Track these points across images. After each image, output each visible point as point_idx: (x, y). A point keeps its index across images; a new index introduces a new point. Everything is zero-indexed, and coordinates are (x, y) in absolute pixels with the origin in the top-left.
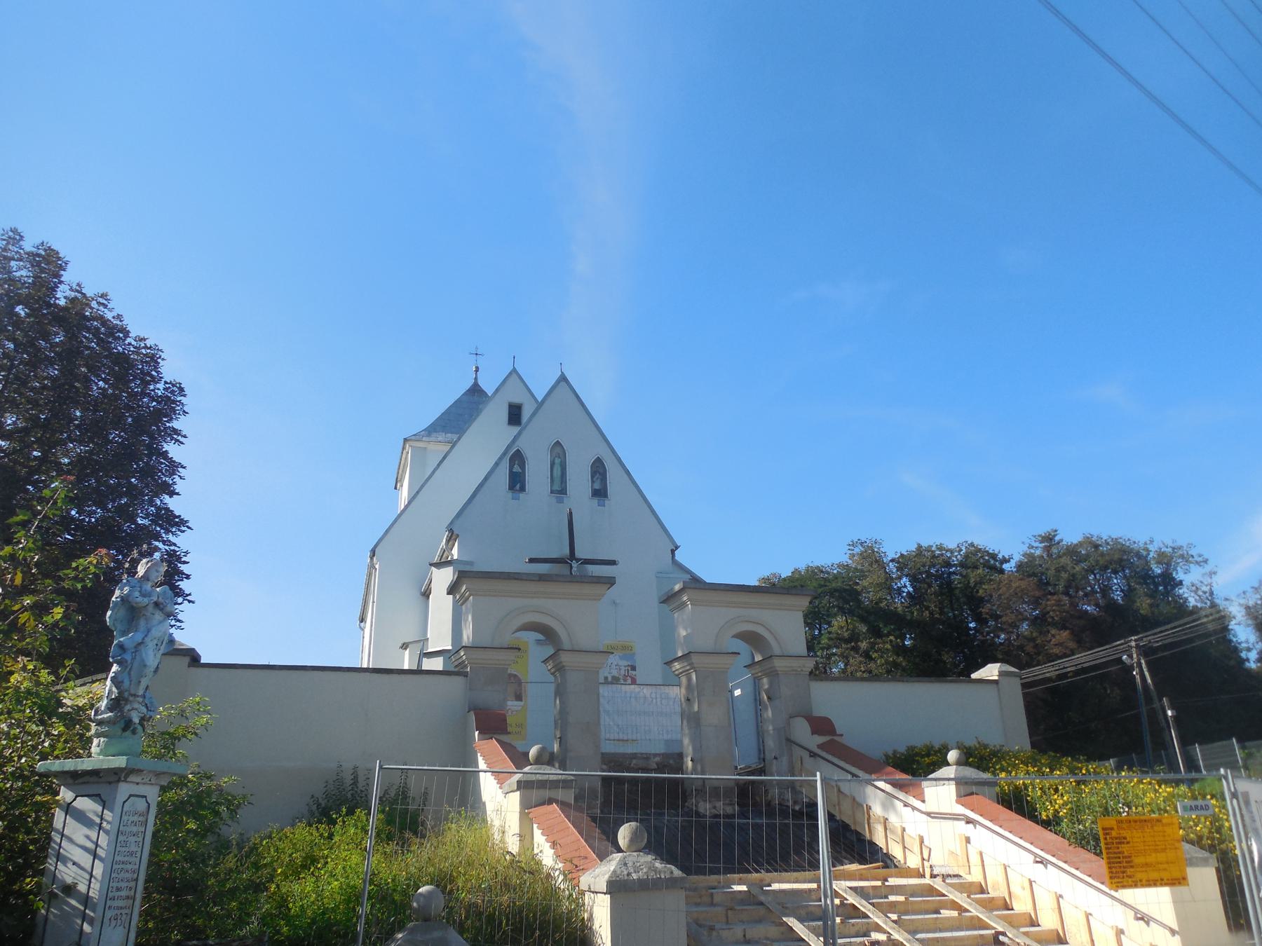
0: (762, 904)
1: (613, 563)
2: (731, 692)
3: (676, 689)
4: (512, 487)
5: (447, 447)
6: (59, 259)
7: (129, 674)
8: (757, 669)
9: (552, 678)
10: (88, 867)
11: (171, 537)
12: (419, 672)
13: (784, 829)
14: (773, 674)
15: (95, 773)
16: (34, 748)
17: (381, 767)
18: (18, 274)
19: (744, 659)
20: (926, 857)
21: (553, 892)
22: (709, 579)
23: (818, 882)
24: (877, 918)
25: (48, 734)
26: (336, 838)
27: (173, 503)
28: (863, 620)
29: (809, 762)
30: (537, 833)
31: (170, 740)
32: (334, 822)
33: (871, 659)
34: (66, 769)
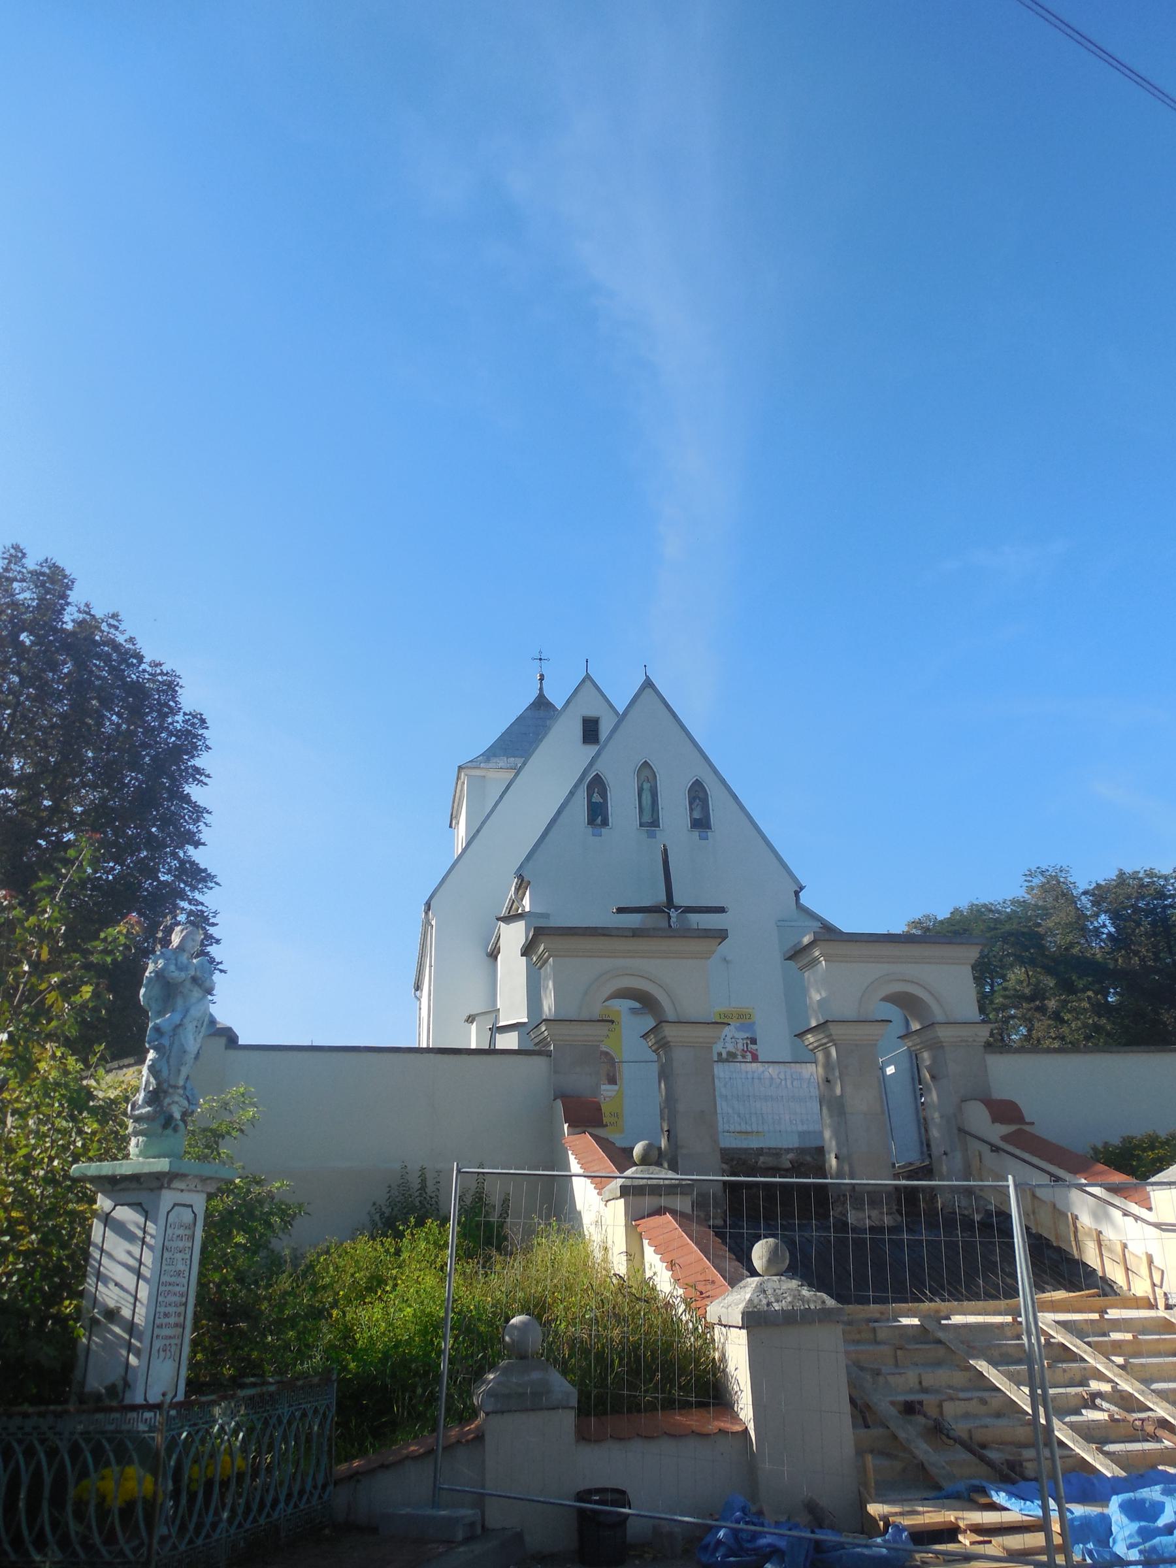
0: (939, 1342)
1: (721, 910)
2: (882, 1069)
3: (811, 1068)
4: (591, 822)
5: (510, 775)
6: (65, 577)
7: (168, 1062)
8: (916, 1039)
9: (655, 1057)
10: (132, 1289)
11: (197, 896)
12: (492, 1052)
13: (969, 1247)
14: (936, 1046)
15: (135, 1178)
16: (65, 1148)
17: (459, 1171)
18: (21, 597)
19: (897, 1028)
20: (1157, 1281)
21: (672, 1326)
22: (847, 925)
23: (1016, 1313)
24: (1094, 1361)
25: (80, 1132)
26: (405, 1255)
27: (196, 855)
28: (1049, 971)
29: (989, 1158)
30: (649, 1251)
31: (213, 1138)
32: (399, 1235)
33: (1062, 1021)
34: (104, 1172)
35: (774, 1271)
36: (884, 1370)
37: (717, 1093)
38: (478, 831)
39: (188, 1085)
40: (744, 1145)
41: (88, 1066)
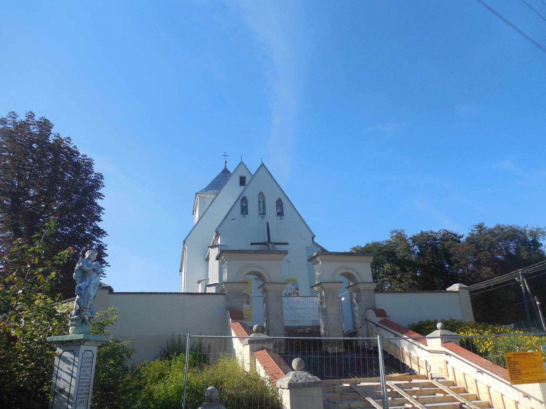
0: (356, 392)
1: (287, 244)
2: (340, 299)
3: (316, 298)
4: (242, 213)
5: (214, 196)
6: (50, 123)
9: (262, 295)
10: (69, 381)
11: (100, 239)
12: (205, 294)
13: (364, 360)
14: (358, 291)
15: (71, 341)
16: (46, 331)
17: (189, 336)
18: (33, 131)
20: (428, 370)
21: (265, 389)
22: (330, 249)
24: (407, 397)
25: (51, 325)
26: (173, 366)
27: (100, 225)
28: (398, 265)
30: (258, 363)
31: (101, 326)
32: (171, 359)
33: (402, 282)
34: (59, 340)
35: (299, 369)
36: (337, 402)
37: (284, 307)
38: (202, 216)
39: (91, 308)
40: (293, 325)
41: (55, 301)
